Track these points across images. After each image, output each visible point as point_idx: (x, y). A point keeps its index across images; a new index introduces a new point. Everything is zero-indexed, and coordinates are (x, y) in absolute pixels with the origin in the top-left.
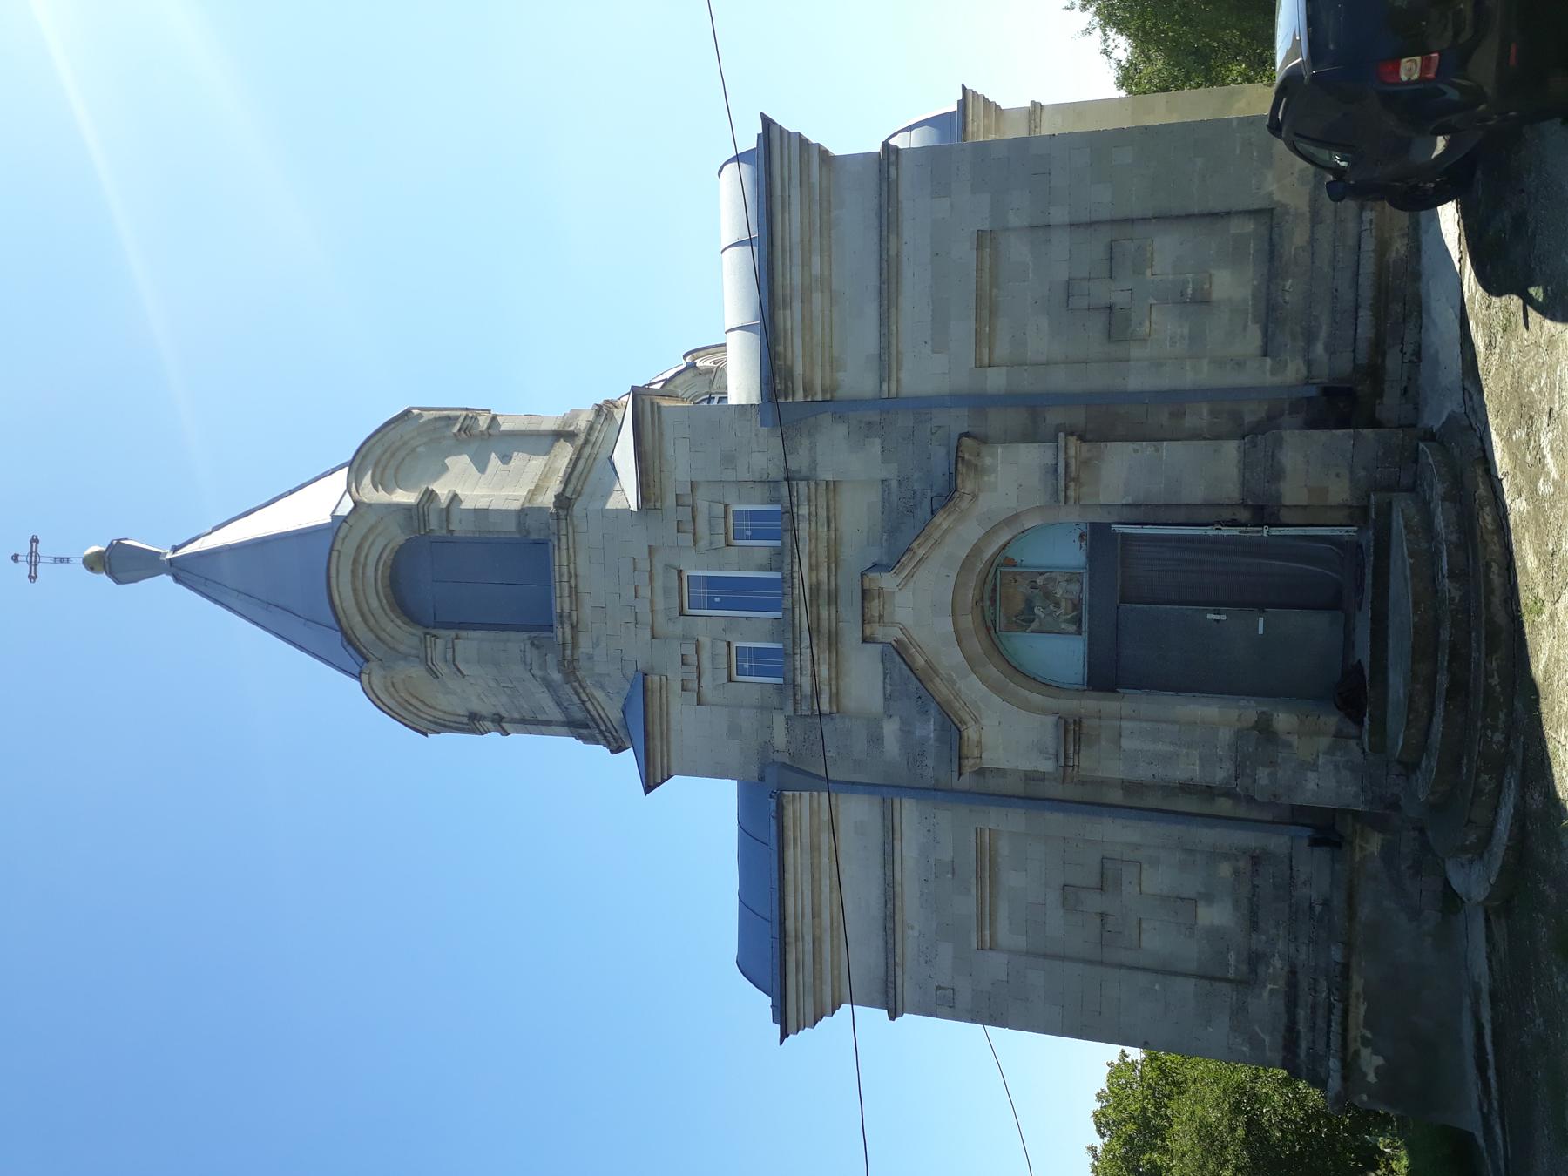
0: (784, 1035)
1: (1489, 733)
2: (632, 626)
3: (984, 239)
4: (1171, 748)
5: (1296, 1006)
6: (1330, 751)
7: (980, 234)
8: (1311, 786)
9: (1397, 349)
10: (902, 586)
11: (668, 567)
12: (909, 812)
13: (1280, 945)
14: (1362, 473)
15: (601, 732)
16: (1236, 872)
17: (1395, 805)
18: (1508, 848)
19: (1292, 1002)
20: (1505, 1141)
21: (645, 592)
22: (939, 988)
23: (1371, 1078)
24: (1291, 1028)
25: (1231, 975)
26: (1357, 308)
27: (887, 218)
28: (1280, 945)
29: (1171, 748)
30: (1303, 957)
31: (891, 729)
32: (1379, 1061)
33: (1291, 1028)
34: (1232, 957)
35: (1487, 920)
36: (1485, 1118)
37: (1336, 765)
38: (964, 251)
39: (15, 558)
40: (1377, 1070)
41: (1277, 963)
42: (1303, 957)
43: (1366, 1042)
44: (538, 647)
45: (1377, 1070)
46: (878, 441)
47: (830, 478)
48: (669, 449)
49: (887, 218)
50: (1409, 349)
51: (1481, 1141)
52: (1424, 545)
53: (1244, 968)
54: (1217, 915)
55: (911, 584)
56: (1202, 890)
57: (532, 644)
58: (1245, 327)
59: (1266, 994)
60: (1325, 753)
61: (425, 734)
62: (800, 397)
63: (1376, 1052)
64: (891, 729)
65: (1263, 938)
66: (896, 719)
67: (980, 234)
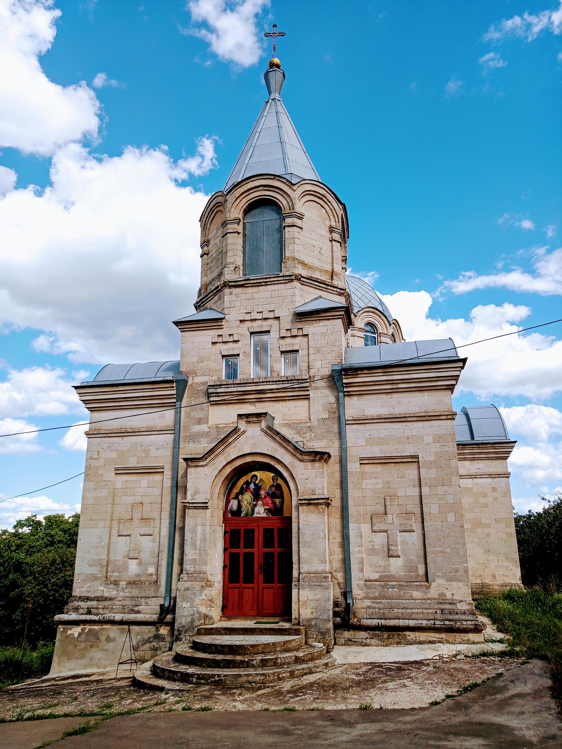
0: (76, 388)
1: (196, 676)
2: (245, 311)
3: (414, 459)
4: (198, 547)
5: (98, 600)
6: (199, 613)
7: (417, 457)
8: (184, 605)
9: (368, 636)
10: (262, 430)
11: (271, 326)
12: (170, 437)
13: (122, 594)
14: (313, 623)
15: (201, 299)
16: (151, 575)
17: (178, 639)
18: (151, 685)
19: (98, 599)
20: (43, 687)
21: (259, 316)
22: (98, 452)
23: (69, 632)
24: (88, 599)
25: (109, 574)
26: (385, 619)
27: (499, 476)
28: (122, 594)
29: (198, 547)
30: (117, 603)
31: (204, 428)
32: (76, 635)
33: (88, 599)
34: (116, 574)
35: (130, 678)
36: (54, 679)
37: (193, 615)
38: (409, 451)
39: (275, 26)
40: (73, 634)
41: (114, 593)
42: (117, 603)
43: (83, 630)
44: (235, 270)
45: (73, 634)
46: (327, 416)
47: (311, 396)
48: (322, 323)
49: (499, 476)
50: (368, 641)
51: (44, 678)
52: (278, 649)
53: (113, 579)
54: (133, 568)
55: (263, 434)
56: (143, 561)
57: (236, 267)
58: (377, 572)
59: (102, 588)
60: (198, 611)
61: (200, 221)
62: (345, 381)
63: (80, 634)
64: (204, 428)
65: (124, 587)
66: (208, 430)
67: (417, 457)
